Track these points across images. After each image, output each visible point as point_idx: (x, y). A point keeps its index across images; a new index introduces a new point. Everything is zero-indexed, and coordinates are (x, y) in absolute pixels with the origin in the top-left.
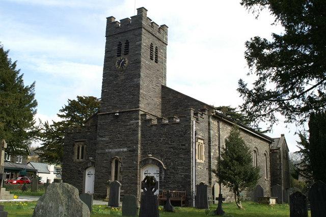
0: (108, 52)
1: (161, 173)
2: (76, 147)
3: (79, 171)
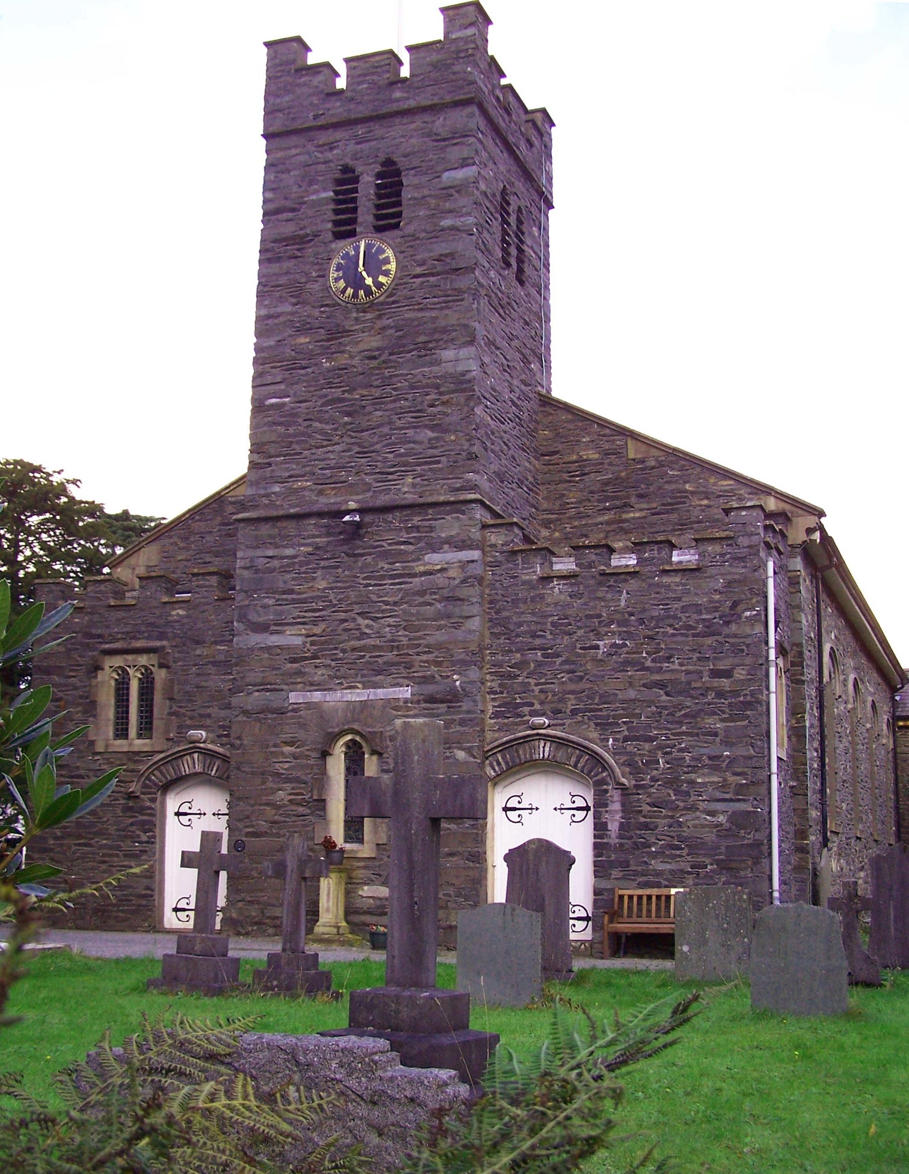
0: (277, 211)
1: (601, 803)
2: (107, 678)
3: (131, 796)
